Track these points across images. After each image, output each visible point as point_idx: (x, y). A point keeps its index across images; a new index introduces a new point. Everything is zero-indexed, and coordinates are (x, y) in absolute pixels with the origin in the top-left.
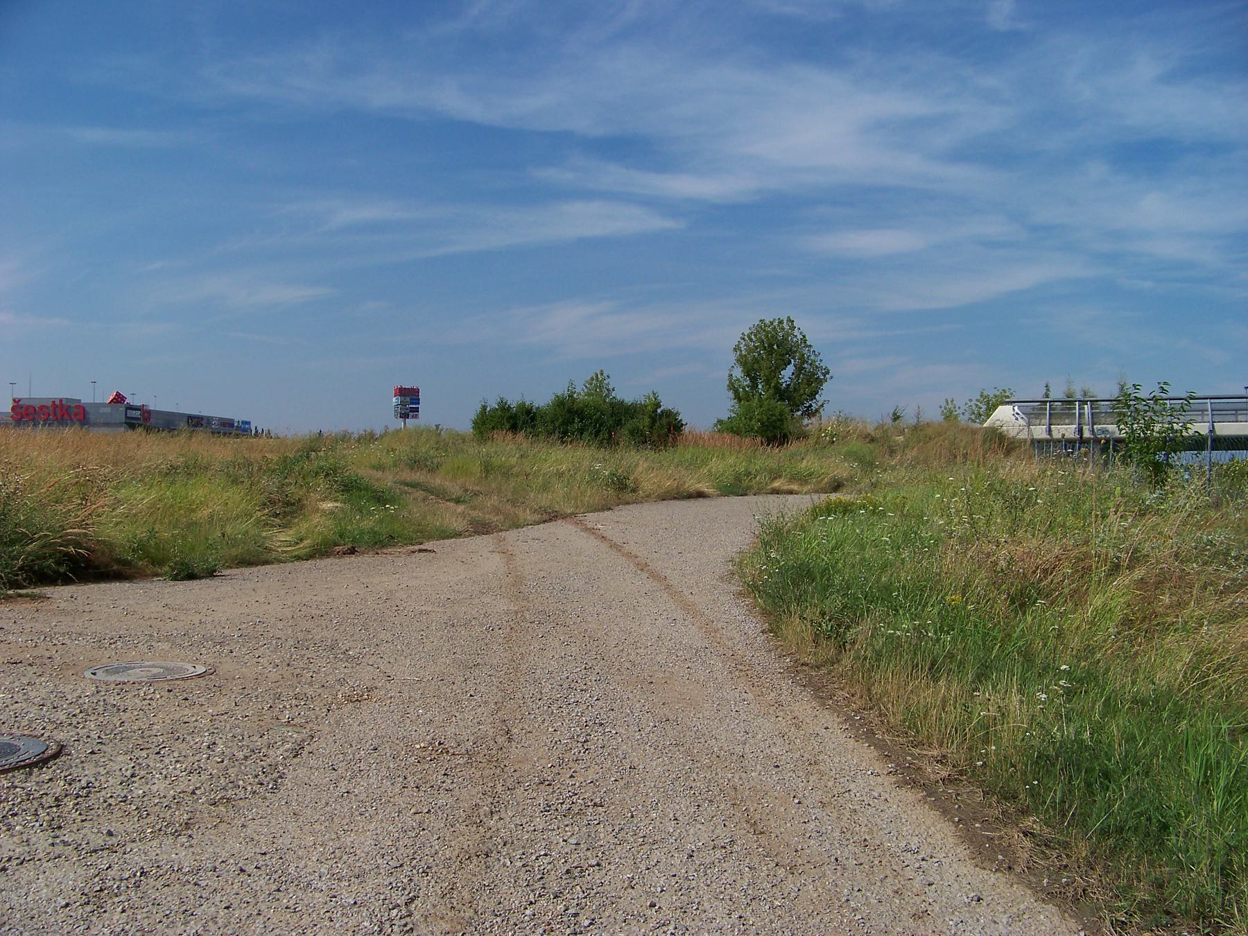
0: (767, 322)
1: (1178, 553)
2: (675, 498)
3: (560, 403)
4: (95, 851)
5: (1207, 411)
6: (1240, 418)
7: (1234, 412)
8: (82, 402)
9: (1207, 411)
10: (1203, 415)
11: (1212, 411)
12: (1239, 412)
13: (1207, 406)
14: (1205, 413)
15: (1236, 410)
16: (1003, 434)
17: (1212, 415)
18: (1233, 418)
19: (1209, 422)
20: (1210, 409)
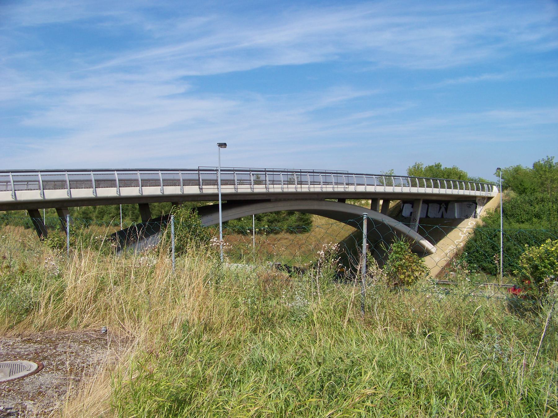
0: (457, 167)
1: (151, 411)
2: (294, 200)
3: (430, 169)
4: (444, 284)
5: (10, 182)
6: (30, 187)
7: (5, 184)
8: (442, 168)
9: (10, 182)
10: (7, 185)
11: (14, 182)
12: (29, 183)
13: (39, 178)
14: (9, 183)
15: (28, 182)
16: (541, 166)
17: (14, 185)
18: (25, 187)
19: (11, 190)
20: (12, 181)
